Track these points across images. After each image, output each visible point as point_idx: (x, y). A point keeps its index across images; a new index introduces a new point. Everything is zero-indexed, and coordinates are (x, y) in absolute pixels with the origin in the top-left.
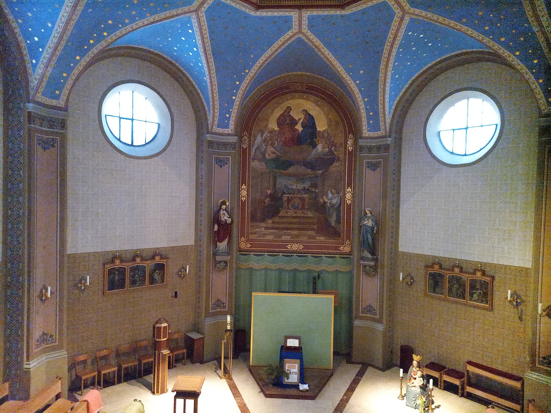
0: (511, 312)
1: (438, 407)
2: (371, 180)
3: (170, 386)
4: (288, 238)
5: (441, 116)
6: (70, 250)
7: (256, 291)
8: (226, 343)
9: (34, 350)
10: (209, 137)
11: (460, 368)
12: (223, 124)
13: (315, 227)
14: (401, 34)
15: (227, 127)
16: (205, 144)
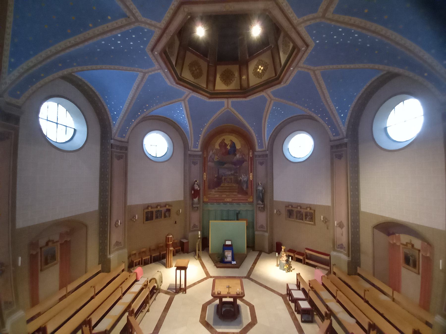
1: (294, 269)
2: (261, 170)
3: (174, 265)
4: (225, 196)
5: (289, 142)
6: (129, 203)
7: (211, 220)
8: (199, 243)
9: (112, 249)
10: (189, 152)
11: (302, 251)
12: (195, 147)
13: (237, 191)
14: (270, 109)
15: (197, 148)
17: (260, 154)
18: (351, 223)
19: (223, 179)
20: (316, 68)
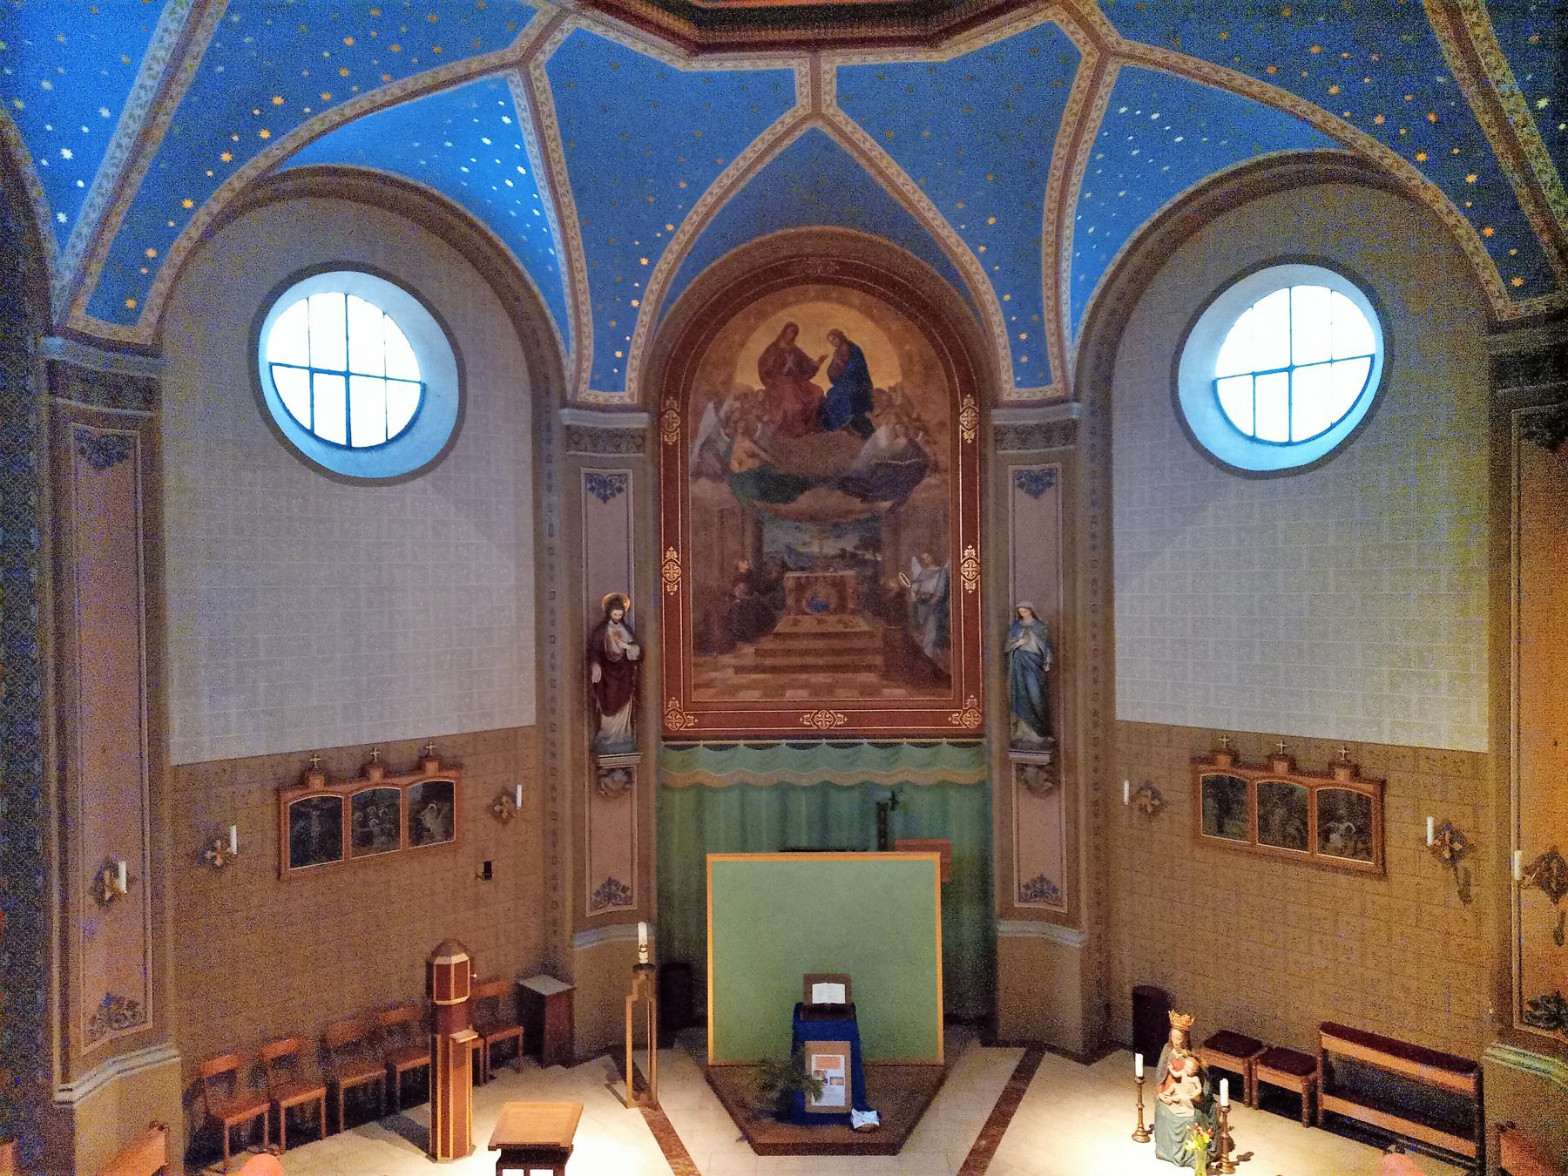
0: (1435, 875)
17: (1029, 419)
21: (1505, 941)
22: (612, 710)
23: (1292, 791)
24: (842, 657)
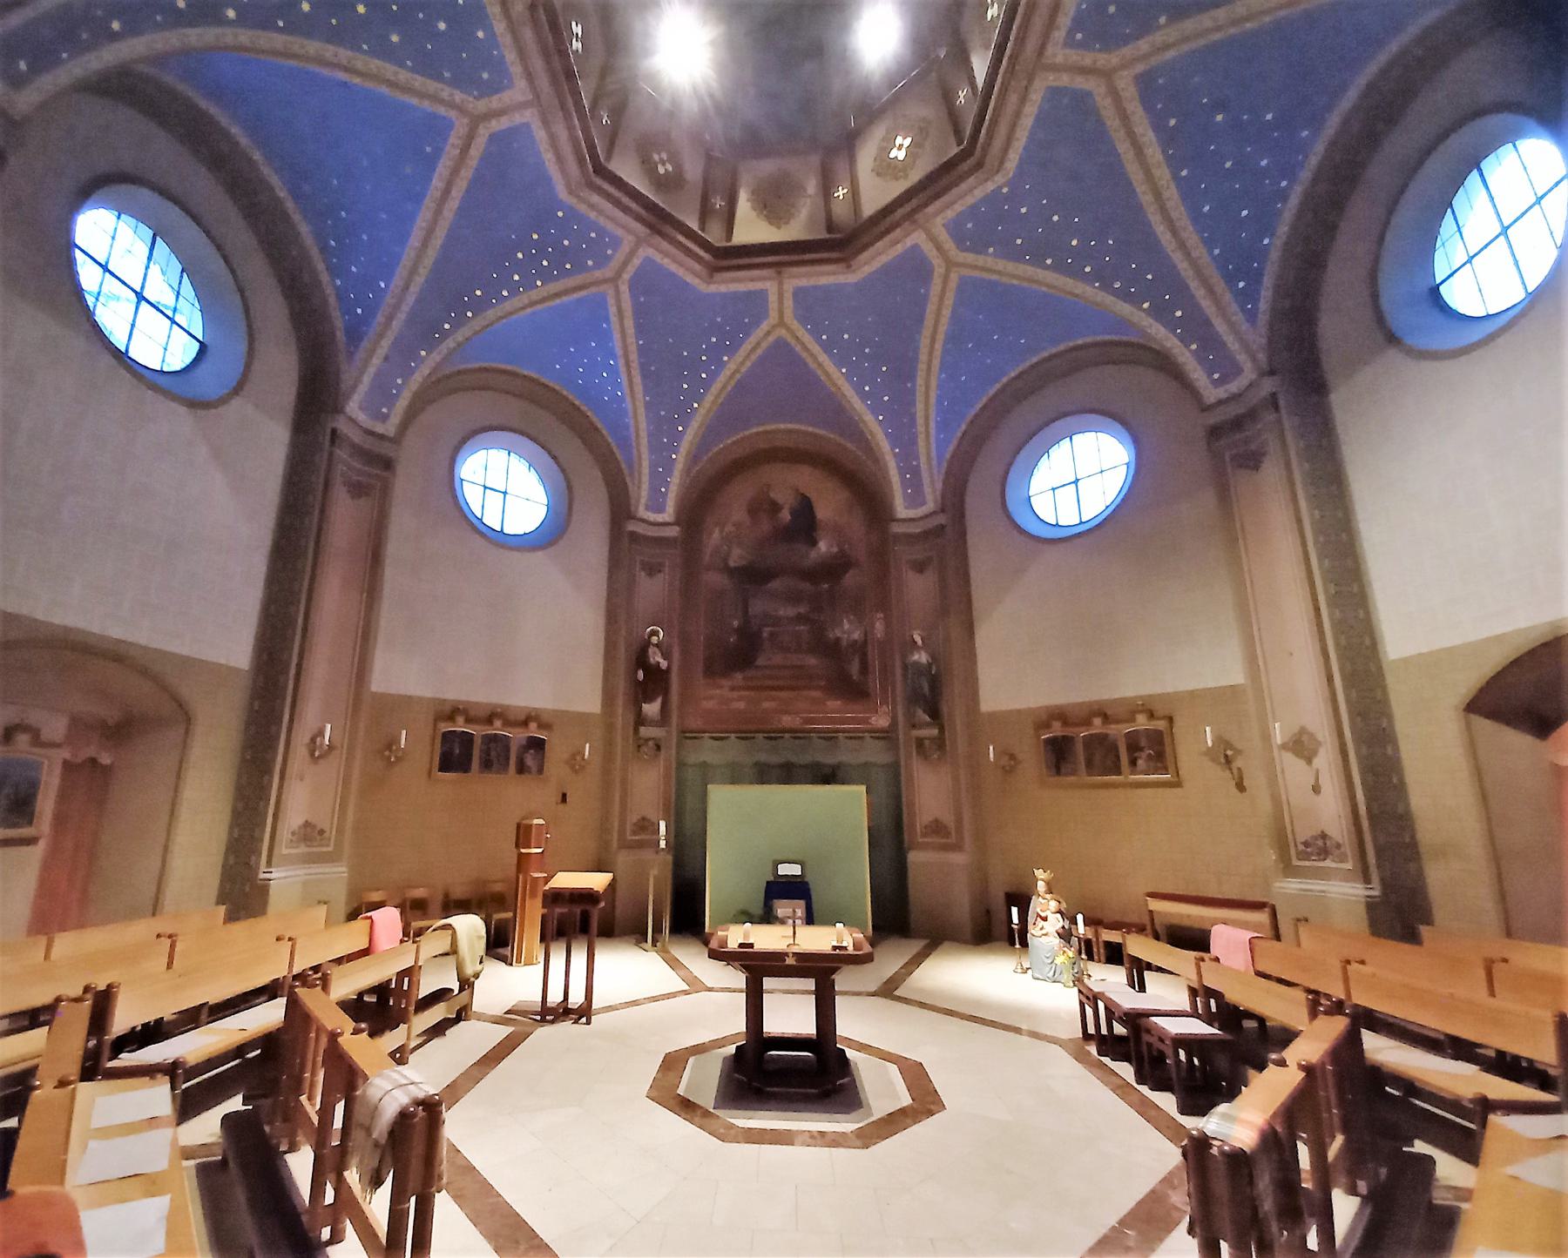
0: (1219, 777)
9: (283, 849)
15: (660, 509)
16: (626, 540)
17: (915, 529)
18: (1352, 720)
19: (765, 635)
20: (1114, 59)
21: (1276, 801)
22: (649, 699)
23: (1107, 735)
24: (799, 680)
